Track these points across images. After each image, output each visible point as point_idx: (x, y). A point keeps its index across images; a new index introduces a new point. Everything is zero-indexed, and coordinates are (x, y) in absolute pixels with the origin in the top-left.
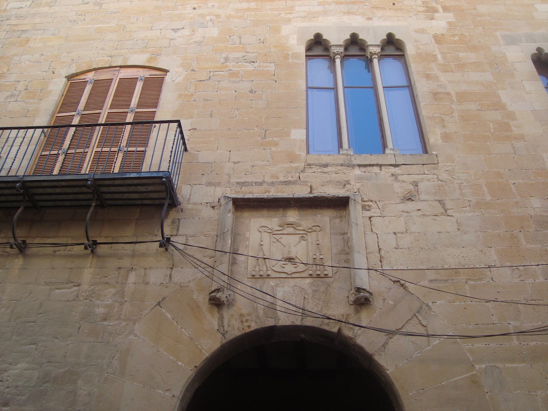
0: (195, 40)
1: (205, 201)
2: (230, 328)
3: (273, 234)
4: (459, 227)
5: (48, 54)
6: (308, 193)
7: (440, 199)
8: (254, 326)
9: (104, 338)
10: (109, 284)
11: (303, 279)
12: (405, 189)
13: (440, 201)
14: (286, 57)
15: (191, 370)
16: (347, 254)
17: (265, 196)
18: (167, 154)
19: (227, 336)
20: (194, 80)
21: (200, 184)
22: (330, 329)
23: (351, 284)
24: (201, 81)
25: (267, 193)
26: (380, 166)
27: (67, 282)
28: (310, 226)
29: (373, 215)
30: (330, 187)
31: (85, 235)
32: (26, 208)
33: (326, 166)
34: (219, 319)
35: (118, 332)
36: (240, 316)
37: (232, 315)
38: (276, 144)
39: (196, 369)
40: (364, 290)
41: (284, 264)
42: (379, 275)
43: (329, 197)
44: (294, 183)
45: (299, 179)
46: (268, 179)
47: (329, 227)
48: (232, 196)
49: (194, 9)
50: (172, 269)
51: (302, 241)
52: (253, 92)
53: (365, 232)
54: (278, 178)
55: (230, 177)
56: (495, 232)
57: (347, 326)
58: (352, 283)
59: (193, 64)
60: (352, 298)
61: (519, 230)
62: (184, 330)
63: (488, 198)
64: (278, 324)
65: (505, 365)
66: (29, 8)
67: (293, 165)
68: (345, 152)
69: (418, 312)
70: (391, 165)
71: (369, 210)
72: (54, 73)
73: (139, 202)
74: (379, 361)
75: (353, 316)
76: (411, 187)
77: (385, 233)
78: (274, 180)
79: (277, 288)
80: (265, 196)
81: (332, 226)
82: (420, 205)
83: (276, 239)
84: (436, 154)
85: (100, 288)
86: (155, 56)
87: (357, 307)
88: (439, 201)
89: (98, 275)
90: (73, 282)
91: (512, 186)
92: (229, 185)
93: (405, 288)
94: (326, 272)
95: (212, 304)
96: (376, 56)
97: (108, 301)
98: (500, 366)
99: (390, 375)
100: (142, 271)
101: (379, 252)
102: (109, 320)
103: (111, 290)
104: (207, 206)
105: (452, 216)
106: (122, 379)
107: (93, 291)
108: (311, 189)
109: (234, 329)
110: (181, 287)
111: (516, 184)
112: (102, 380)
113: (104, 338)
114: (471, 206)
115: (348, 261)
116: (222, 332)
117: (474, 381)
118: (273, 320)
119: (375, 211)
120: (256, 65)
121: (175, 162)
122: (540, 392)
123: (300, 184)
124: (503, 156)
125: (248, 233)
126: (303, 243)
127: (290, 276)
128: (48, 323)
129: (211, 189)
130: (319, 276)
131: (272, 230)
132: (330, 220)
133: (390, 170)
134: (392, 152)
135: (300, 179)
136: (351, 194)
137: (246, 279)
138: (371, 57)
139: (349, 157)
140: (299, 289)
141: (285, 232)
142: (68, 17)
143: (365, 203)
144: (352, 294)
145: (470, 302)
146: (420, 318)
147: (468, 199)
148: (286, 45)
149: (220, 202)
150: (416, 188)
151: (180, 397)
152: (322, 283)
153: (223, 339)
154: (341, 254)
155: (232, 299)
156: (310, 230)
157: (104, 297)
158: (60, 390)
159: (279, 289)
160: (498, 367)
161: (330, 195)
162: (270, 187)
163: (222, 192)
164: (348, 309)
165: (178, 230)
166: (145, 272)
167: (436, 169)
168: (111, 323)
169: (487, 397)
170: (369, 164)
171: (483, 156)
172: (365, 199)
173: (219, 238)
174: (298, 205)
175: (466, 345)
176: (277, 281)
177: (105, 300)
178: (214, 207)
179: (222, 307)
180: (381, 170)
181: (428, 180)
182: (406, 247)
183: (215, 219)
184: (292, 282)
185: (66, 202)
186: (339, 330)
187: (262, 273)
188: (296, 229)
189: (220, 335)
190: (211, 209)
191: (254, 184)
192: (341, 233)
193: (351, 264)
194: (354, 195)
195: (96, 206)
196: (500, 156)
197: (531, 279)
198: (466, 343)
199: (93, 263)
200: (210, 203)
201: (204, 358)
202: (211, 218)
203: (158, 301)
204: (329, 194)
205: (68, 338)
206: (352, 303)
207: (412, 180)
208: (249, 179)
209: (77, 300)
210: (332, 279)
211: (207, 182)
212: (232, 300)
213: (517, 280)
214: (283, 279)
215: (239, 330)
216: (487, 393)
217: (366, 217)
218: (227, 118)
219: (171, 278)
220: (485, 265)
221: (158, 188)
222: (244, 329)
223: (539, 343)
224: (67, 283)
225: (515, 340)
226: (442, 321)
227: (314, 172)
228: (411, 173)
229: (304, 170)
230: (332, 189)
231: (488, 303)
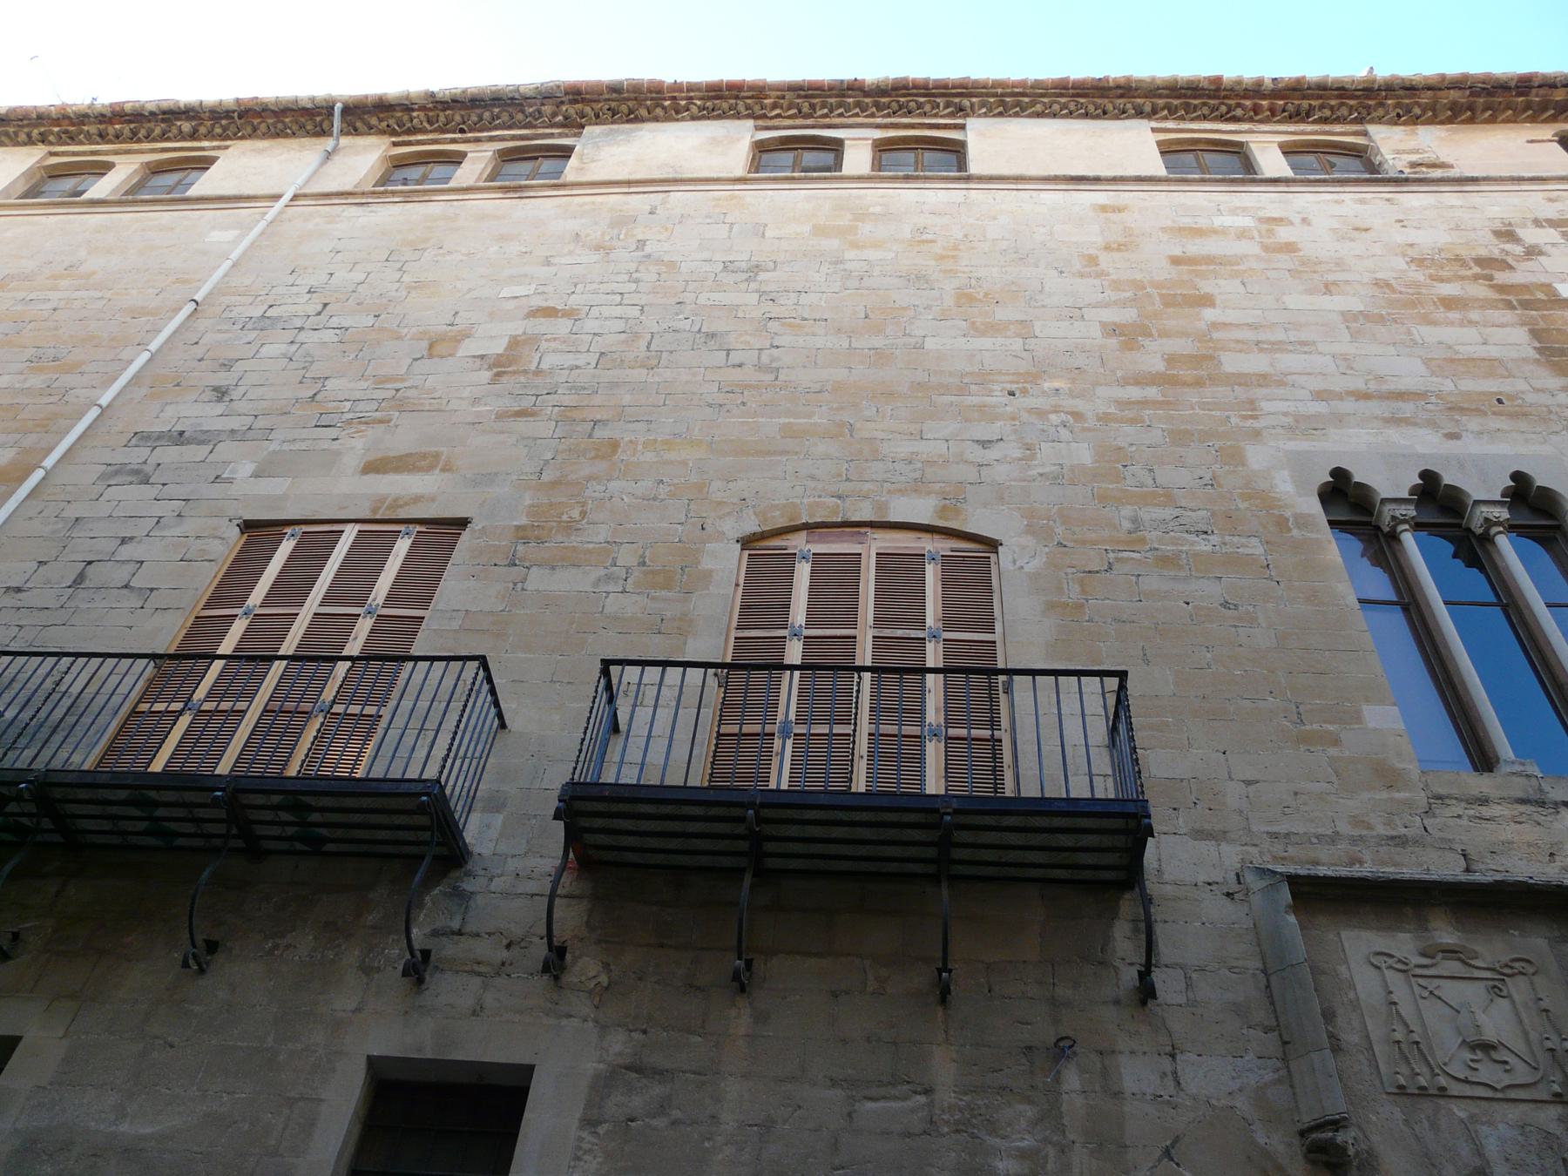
0: (1041, 471)
1: (1202, 878)
5: (676, 481)
14: (1282, 523)
20: (1074, 570)
24: (1090, 572)
32: (435, 858)
33: (1484, 801)
38: (1336, 741)
41: (1472, 1060)
49: (1012, 394)
52: (1231, 606)
59: (1056, 530)
66: (596, 368)
72: (703, 529)
83: (1426, 988)
86: (953, 499)
90: (908, 1082)
95: (1314, 1163)
96: (1407, 527)
120: (1215, 539)
129: (1207, 848)
130: (1403, 1091)
131: (1406, 964)
135: (1426, 831)
138: (1394, 527)
142: (701, 394)
148: (1273, 495)
163: (1241, 857)
176: (1474, 1108)
177: (1014, 1137)
178: (1232, 894)
188: (1470, 965)
190: (1227, 901)
191: (1315, 840)
218: (1187, 669)
224: (893, 1085)
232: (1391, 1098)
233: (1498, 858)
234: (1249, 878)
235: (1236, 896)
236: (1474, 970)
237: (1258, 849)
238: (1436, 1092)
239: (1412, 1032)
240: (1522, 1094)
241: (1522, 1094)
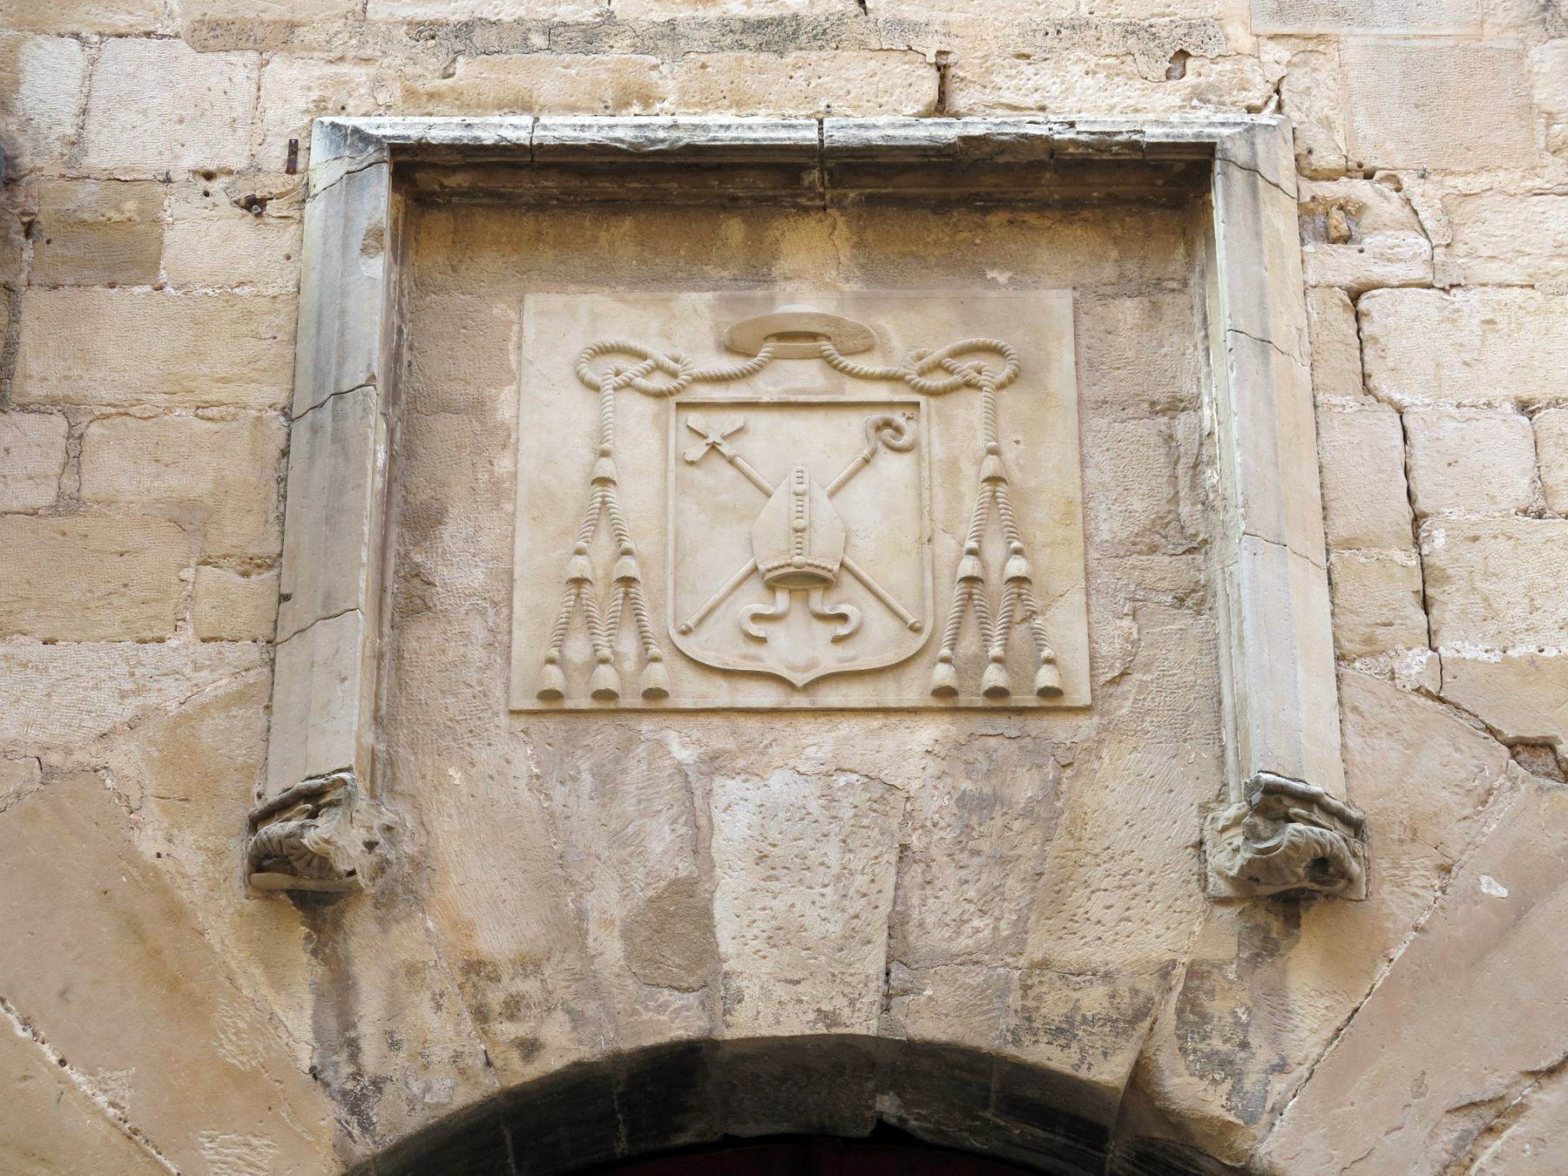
41: (757, 618)
95: (268, 894)
126: (893, 467)
130: (555, 706)
131: (674, 375)
163: (314, 95)
178: (262, 202)
190: (243, 224)
191: (538, 40)
210: (1086, 726)
232: (520, 724)
233: (1030, 71)
234: (323, 167)
235: (271, 207)
236: (847, 380)
237: (371, 70)
238: (638, 703)
239: (627, 553)
240: (854, 695)
241: (854, 695)
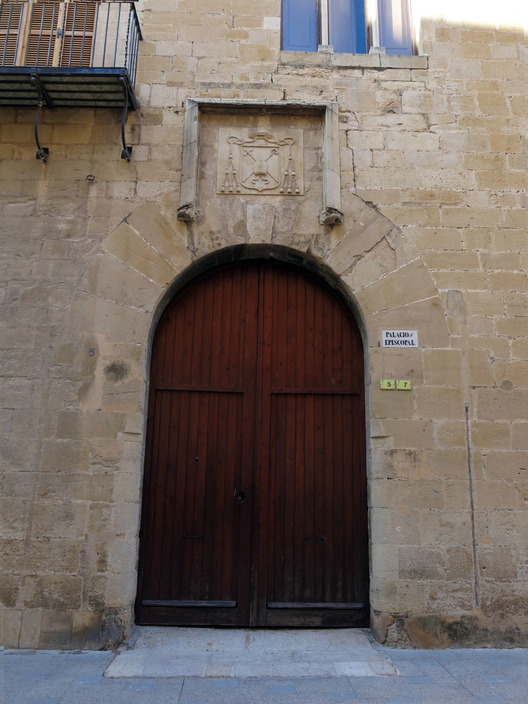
2: (200, 246)
3: (243, 147)
4: (441, 145)
6: (281, 99)
7: (425, 113)
8: (224, 244)
9: (70, 255)
10: (68, 197)
11: (274, 196)
12: (388, 98)
13: (424, 114)
15: (163, 287)
16: (319, 171)
17: (234, 101)
18: (122, 46)
19: (197, 254)
21: (160, 84)
22: (299, 249)
23: (323, 204)
25: (236, 98)
26: (363, 69)
27: (21, 195)
28: (282, 139)
29: (350, 128)
30: (306, 93)
31: (35, 141)
33: (302, 67)
34: (188, 236)
35: (85, 249)
36: (210, 233)
37: (202, 233)
39: (167, 286)
40: (336, 210)
42: (352, 195)
43: (304, 105)
44: (266, 86)
45: (271, 82)
46: (237, 81)
47: (302, 140)
48: (198, 101)
50: (136, 182)
51: (274, 156)
53: (340, 148)
54: (248, 79)
55: (194, 76)
56: (478, 153)
57: (316, 246)
58: (323, 202)
60: (323, 218)
61: (506, 152)
62: (153, 247)
63: (478, 113)
64: (249, 242)
65: (468, 290)
67: (265, 64)
68: (324, 49)
69: (388, 234)
70: (375, 68)
71: (346, 122)
73: (92, 103)
74: (346, 282)
75: (323, 236)
76: (394, 97)
77: (361, 150)
78: (244, 82)
79: (248, 205)
80: (234, 102)
81: (306, 139)
82: (402, 119)
84: (427, 56)
85: (59, 202)
87: (327, 227)
88: (424, 115)
89: (55, 188)
91: (508, 101)
92: (194, 86)
93: (377, 209)
94: (297, 190)
95: (181, 221)
97: (70, 216)
98: (462, 291)
99: (356, 296)
100: (104, 184)
101: (354, 170)
102: (73, 236)
103: (71, 204)
104: (169, 110)
105: (435, 133)
106: (94, 296)
107: (52, 205)
108: (284, 94)
109: (204, 247)
110: (147, 202)
111: (512, 97)
112: (73, 297)
113: (70, 255)
114: (457, 121)
115: (321, 179)
116: (193, 250)
117: (436, 304)
118: (243, 238)
119: (352, 124)
121: (136, 56)
122: (496, 316)
123: (272, 88)
124: (504, 62)
125: (216, 144)
126: (275, 157)
127: (261, 193)
128: (6, 240)
131: (242, 142)
132: (304, 131)
133: (373, 75)
134: (377, 52)
136: (328, 103)
137: (216, 195)
139: (328, 56)
140: (270, 207)
141: (256, 144)
143: (343, 114)
144: (323, 214)
145: (442, 228)
146: (390, 241)
147: (456, 113)
149: (184, 106)
150: (400, 98)
151: (153, 313)
152: (293, 201)
153: (194, 256)
154: (314, 171)
155: (202, 216)
156: (282, 143)
157: (65, 213)
158: (31, 307)
159: (249, 206)
160: (459, 292)
161: (305, 103)
162: (240, 90)
163: (186, 94)
164: (318, 229)
165: (139, 139)
166: (107, 186)
167: (425, 75)
168: (76, 239)
169: (446, 319)
170: (350, 65)
171: (481, 62)
172: (343, 109)
173: (185, 149)
174: (270, 113)
175: (432, 269)
176: (248, 198)
177: (67, 215)
178: (178, 112)
179: (192, 224)
180: (363, 74)
181: (414, 89)
182: (382, 166)
183: (180, 127)
184: (263, 199)
185: (4, 100)
186: (309, 250)
187: (231, 189)
189: (190, 254)
190: (175, 115)
191: (221, 86)
192: (315, 148)
193: (324, 182)
194: (332, 104)
195: (43, 106)
196: (501, 62)
197: (507, 206)
198: (433, 268)
199: (47, 175)
200: (173, 107)
201: (175, 275)
202: (175, 125)
203: (124, 217)
204: (304, 102)
205: (31, 255)
206: (322, 223)
207: (396, 88)
208: (216, 80)
209: (35, 215)
210: (303, 198)
211: (168, 81)
212: (201, 217)
213: (493, 207)
214: (253, 196)
215: (209, 248)
216: (446, 315)
217: (343, 130)
219: (136, 193)
220: (463, 189)
221: (114, 88)
222: (215, 247)
223: (504, 271)
225: (481, 267)
226: (411, 245)
227: (289, 74)
228: (397, 80)
229: (277, 70)
230: (307, 95)
231: (459, 229)
